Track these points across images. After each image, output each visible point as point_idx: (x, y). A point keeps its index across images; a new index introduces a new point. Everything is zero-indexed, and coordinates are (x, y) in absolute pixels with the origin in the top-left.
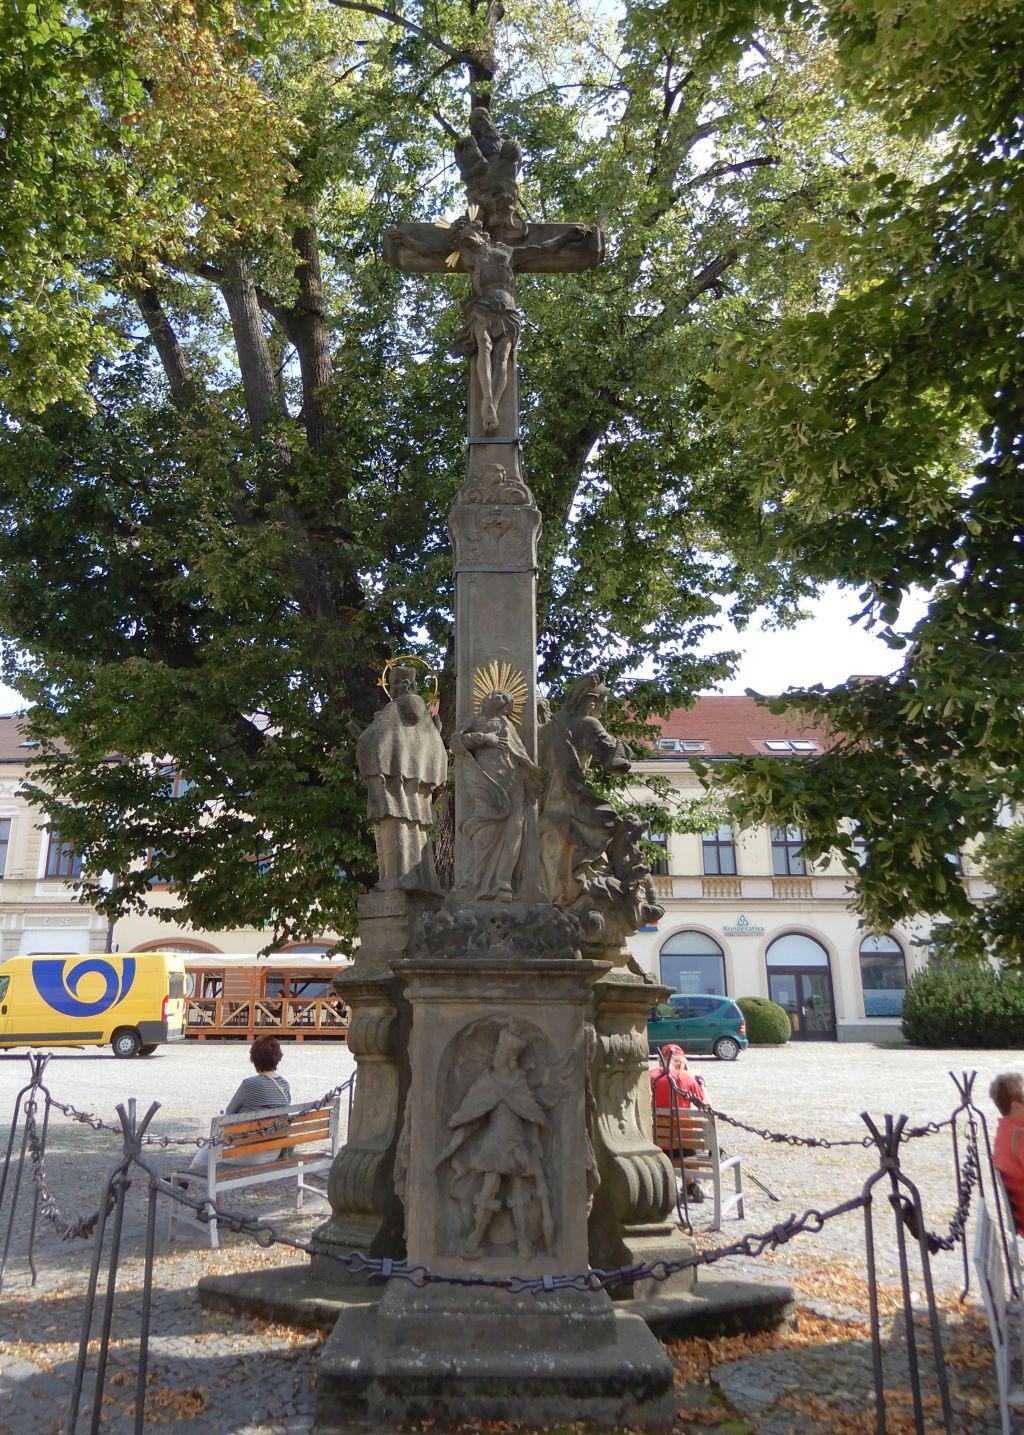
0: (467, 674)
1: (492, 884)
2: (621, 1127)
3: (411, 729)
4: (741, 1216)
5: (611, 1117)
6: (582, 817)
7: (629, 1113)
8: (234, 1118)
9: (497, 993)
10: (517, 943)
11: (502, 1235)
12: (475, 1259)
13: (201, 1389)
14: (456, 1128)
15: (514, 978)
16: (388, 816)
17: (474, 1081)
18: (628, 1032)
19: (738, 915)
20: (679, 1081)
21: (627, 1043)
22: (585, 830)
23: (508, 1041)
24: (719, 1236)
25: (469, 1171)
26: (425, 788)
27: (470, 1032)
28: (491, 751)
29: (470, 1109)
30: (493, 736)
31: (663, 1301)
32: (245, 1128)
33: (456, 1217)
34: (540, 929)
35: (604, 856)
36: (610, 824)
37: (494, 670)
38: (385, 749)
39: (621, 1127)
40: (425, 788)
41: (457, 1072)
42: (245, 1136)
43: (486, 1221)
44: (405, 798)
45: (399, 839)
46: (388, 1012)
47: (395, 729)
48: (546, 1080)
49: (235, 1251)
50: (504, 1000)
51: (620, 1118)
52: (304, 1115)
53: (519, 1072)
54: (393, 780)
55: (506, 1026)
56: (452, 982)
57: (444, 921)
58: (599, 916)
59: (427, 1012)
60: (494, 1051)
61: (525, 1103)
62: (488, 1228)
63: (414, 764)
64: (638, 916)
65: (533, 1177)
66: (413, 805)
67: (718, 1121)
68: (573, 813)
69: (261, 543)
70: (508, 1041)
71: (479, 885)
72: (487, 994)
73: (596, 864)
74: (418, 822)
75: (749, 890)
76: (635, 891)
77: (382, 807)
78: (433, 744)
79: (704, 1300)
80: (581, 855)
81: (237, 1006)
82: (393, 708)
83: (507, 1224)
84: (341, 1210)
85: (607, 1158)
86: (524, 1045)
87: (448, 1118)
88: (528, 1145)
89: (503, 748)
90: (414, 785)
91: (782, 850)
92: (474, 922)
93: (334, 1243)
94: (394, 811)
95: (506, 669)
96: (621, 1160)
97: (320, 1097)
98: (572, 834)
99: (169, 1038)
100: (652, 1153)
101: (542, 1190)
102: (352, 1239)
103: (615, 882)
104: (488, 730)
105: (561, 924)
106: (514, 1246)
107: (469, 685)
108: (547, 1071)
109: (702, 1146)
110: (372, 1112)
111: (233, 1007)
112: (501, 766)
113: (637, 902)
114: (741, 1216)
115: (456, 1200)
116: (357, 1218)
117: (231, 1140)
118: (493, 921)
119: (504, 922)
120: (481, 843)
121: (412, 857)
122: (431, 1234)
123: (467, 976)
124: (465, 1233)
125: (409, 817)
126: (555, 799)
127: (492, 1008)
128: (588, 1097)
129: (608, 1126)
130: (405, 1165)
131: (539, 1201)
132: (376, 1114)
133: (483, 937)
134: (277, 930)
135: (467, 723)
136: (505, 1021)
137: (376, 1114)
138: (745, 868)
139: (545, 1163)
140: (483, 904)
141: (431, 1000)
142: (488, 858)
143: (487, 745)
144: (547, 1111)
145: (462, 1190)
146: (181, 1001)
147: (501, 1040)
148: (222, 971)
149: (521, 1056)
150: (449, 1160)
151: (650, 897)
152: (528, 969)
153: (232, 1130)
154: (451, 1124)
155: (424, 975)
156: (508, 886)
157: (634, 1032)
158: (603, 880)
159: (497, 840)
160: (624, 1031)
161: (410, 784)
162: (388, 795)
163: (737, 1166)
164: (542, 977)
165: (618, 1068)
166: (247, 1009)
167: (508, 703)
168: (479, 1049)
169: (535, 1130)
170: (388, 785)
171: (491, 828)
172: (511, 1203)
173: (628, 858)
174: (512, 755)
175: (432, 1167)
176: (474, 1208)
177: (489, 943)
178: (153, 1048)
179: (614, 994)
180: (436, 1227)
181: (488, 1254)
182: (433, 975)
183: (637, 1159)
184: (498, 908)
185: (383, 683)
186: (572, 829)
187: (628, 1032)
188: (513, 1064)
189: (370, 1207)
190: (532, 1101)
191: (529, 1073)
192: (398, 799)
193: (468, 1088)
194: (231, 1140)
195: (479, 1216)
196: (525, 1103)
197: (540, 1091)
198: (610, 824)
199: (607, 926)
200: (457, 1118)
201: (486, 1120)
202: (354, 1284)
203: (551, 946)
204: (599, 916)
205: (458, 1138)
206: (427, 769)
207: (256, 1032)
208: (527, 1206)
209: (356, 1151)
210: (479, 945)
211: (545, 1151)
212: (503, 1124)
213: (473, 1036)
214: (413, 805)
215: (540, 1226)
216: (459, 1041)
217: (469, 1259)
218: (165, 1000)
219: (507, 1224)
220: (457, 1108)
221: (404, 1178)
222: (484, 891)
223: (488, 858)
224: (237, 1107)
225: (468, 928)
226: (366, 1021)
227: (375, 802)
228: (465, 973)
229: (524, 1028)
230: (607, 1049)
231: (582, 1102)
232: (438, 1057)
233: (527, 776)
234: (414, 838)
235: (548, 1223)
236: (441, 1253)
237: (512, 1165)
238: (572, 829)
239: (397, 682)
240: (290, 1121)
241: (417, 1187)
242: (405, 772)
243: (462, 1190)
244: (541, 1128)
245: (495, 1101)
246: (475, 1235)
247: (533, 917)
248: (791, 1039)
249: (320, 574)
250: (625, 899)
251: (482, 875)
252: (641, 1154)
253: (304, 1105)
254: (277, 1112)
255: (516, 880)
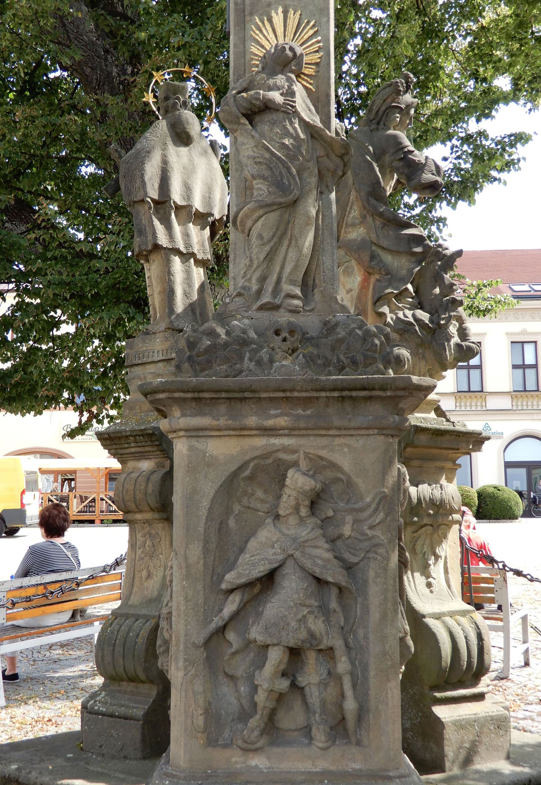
0: (242, 24)
1: (276, 291)
2: (429, 585)
3: (183, 150)
4: (527, 664)
5: (417, 575)
6: (385, 243)
7: (437, 570)
8: (19, 582)
9: (282, 421)
10: (310, 360)
11: (291, 719)
12: (256, 750)
13: (99, 744)
14: (231, 591)
15: (307, 402)
16: (157, 247)
17: (253, 533)
18: (437, 482)
19: (484, 422)
20: (469, 540)
21: (437, 494)
22: (388, 258)
23: (297, 481)
24: (509, 684)
25: (248, 643)
26: (201, 218)
27: (247, 473)
28: (274, 116)
29: (252, 564)
30: (276, 97)
31: (477, 772)
32: (30, 592)
33: (231, 698)
34: (341, 341)
35: (410, 287)
36: (419, 249)
37: (278, 19)
38: (151, 170)
39: (429, 585)
40: (201, 218)
41: (232, 523)
42: (29, 599)
43: (271, 705)
44: (177, 228)
45: (169, 273)
46: (160, 465)
47: (164, 148)
48: (347, 530)
49: (23, 709)
50: (291, 431)
51: (428, 576)
52: (92, 578)
53: (312, 521)
54: (163, 204)
55: (295, 464)
56: (223, 408)
57: (212, 333)
58: (404, 353)
59: (191, 448)
60: (279, 497)
61: (320, 558)
62: (273, 713)
63: (188, 189)
64: (450, 354)
65: (331, 649)
66: (187, 235)
67: (510, 575)
68: (373, 236)
69: (47, 38)
70: (297, 481)
71: (259, 292)
72: (270, 423)
73: (401, 295)
74: (193, 255)
75: (492, 403)
76: (447, 325)
77: (150, 237)
78: (210, 169)
79: (526, 770)
80: (382, 288)
81: (86, 498)
82: (162, 126)
83: (297, 705)
84: (112, 679)
85: (416, 618)
86: (319, 486)
87: (221, 579)
88: (324, 610)
89: (289, 111)
90: (187, 213)
91: (520, 371)
92: (252, 335)
93: (103, 715)
94: (163, 240)
95: (293, 19)
96: (429, 621)
97: (111, 561)
98: (372, 264)
99: (28, 522)
100: (464, 613)
101: (343, 665)
102: (122, 711)
103: (424, 316)
104: (270, 89)
105: (368, 334)
106: (307, 731)
107: (243, 41)
108: (349, 519)
109: (492, 601)
110: (144, 573)
111: (82, 499)
112: (287, 134)
113: (449, 338)
114: (527, 664)
115: (232, 678)
116: (130, 687)
117: (14, 604)
118: (277, 333)
119: (292, 332)
120: (260, 237)
121: (186, 294)
122: (200, 721)
123: (242, 400)
124: (244, 716)
125: (183, 249)
126: (353, 225)
127: (276, 441)
128: (401, 550)
129: (415, 586)
130: (166, 635)
131: (339, 678)
132: (149, 576)
133: (264, 354)
134: (81, 414)
135: (243, 83)
136: (294, 457)
137: (149, 576)
138: (489, 387)
139: (345, 632)
140: (265, 314)
141: (194, 433)
142: (270, 257)
143: (268, 107)
144: (349, 567)
145: (240, 667)
146: (37, 494)
147: (288, 481)
148: (74, 472)
149: (315, 502)
150: (222, 630)
151: (463, 333)
152: (323, 390)
153: (18, 593)
154: (224, 586)
155: (185, 400)
156: (298, 291)
157: (443, 481)
158: (409, 313)
159: (283, 234)
160: (433, 481)
161: (184, 213)
162: (156, 223)
163: (524, 619)
164: (343, 398)
165: (426, 521)
166: (94, 500)
167: (297, 58)
168: (260, 494)
169: (334, 591)
170: (157, 212)
171: (273, 217)
172: (302, 681)
173: (437, 290)
174: (302, 121)
175: (200, 639)
176: (255, 688)
177: (271, 361)
178: (16, 530)
179: (423, 438)
180: (206, 712)
181: (273, 743)
182: (197, 400)
183: (447, 619)
184: (283, 318)
185: (149, 98)
186: (373, 257)
187: (437, 482)
188: (304, 512)
189: (142, 676)
190: (329, 555)
191: (326, 522)
192: (169, 227)
193: (247, 542)
194: (14, 604)
195: (261, 698)
196: (320, 558)
197: (339, 543)
198: (419, 249)
199: (414, 365)
200: (231, 578)
201: (269, 580)
202: (125, 757)
203: (354, 363)
204: (404, 353)
205: (231, 606)
206: (204, 197)
207: (102, 518)
208: (323, 684)
209: (127, 616)
210: (259, 363)
211: (346, 619)
212: (291, 586)
213: (251, 478)
214: (187, 235)
215: (340, 708)
216: (233, 485)
217: (249, 749)
218: (23, 492)
219: (297, 705)
220: (231, 568)
221: (167, 650)
222: (266, 298)
223: (270, 257)
224: (25, 572)
225: (244, 342)
226: (134, 475)
227: (141, 233)
228: (239, 397)
229: (318, 465)
230: (415, 501)
231: (395, 558)
232: (205, 504)
233: (321, 152)
234: (188, 274)
235: (350, 705)
236: (212, 742)
237: (303, 635)
238: (373, 257)
239: (167, 98)
240: (78, 585)
241: (181, 664)
242: (177, 195)
243: (240, 667)
244: (340, 589)
245: (280, 557)
246: (255, 722)
247: (329, 328)
248: (523, 516)
249: (106, 60)
250: (435, 333)
251: (263, 279)
252: (452, 614)
253: (94, 569)
254: (64, 576)
255: (307, 285)
